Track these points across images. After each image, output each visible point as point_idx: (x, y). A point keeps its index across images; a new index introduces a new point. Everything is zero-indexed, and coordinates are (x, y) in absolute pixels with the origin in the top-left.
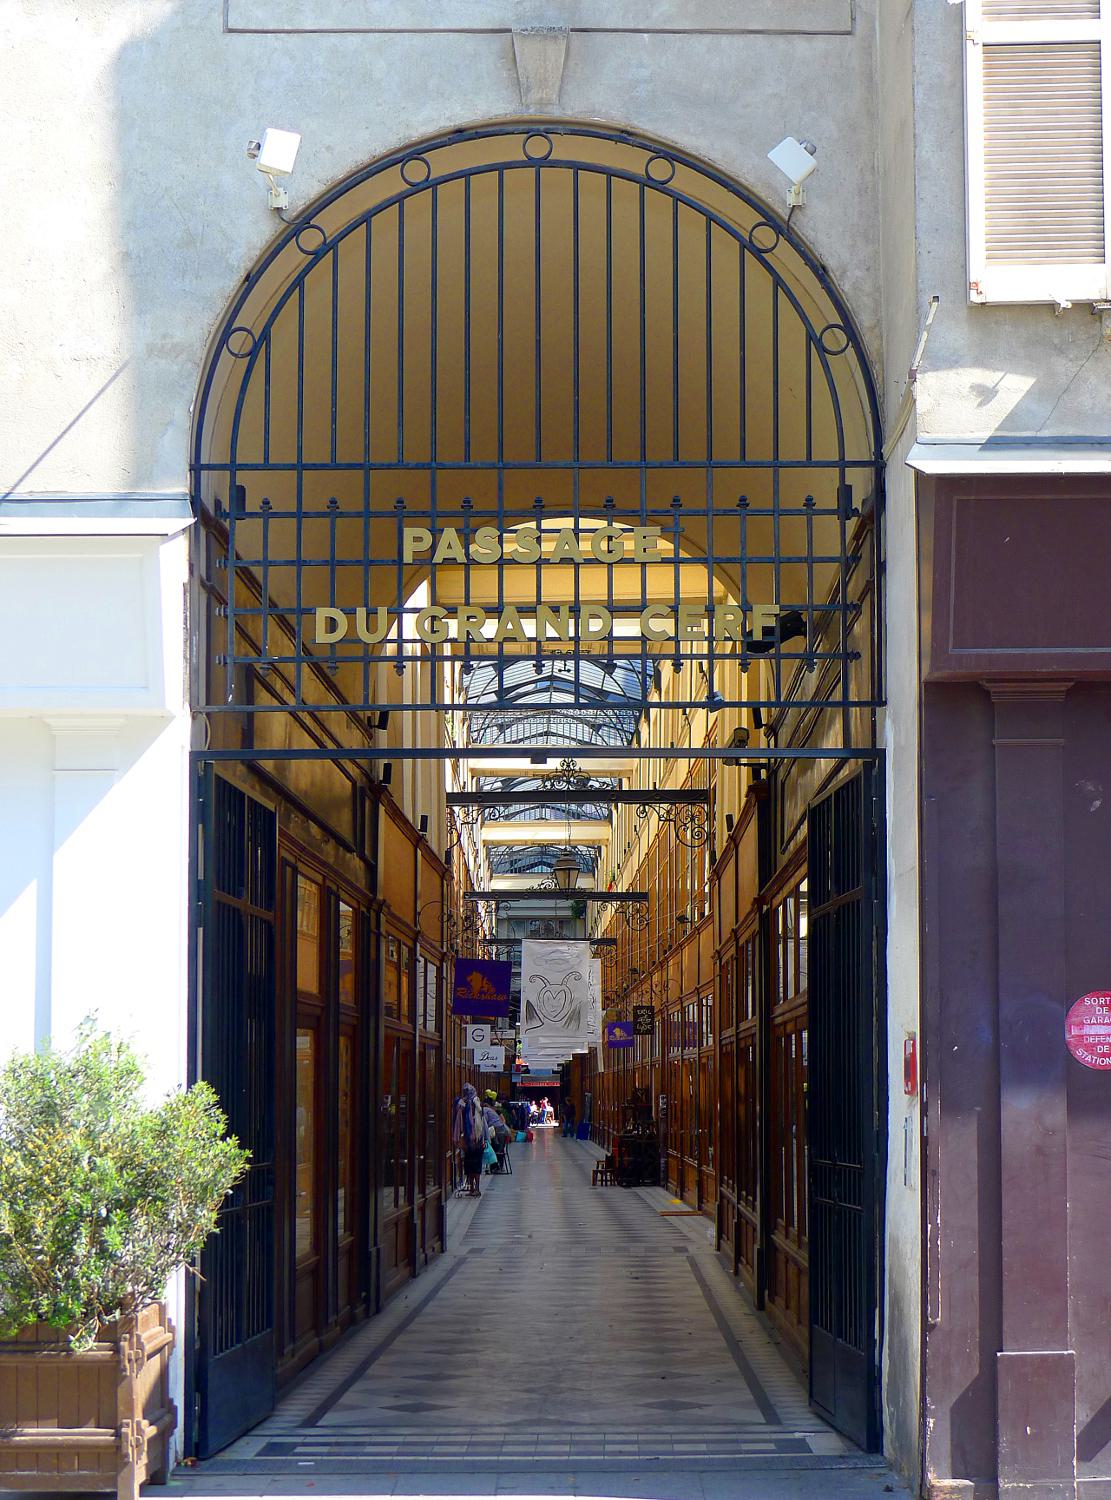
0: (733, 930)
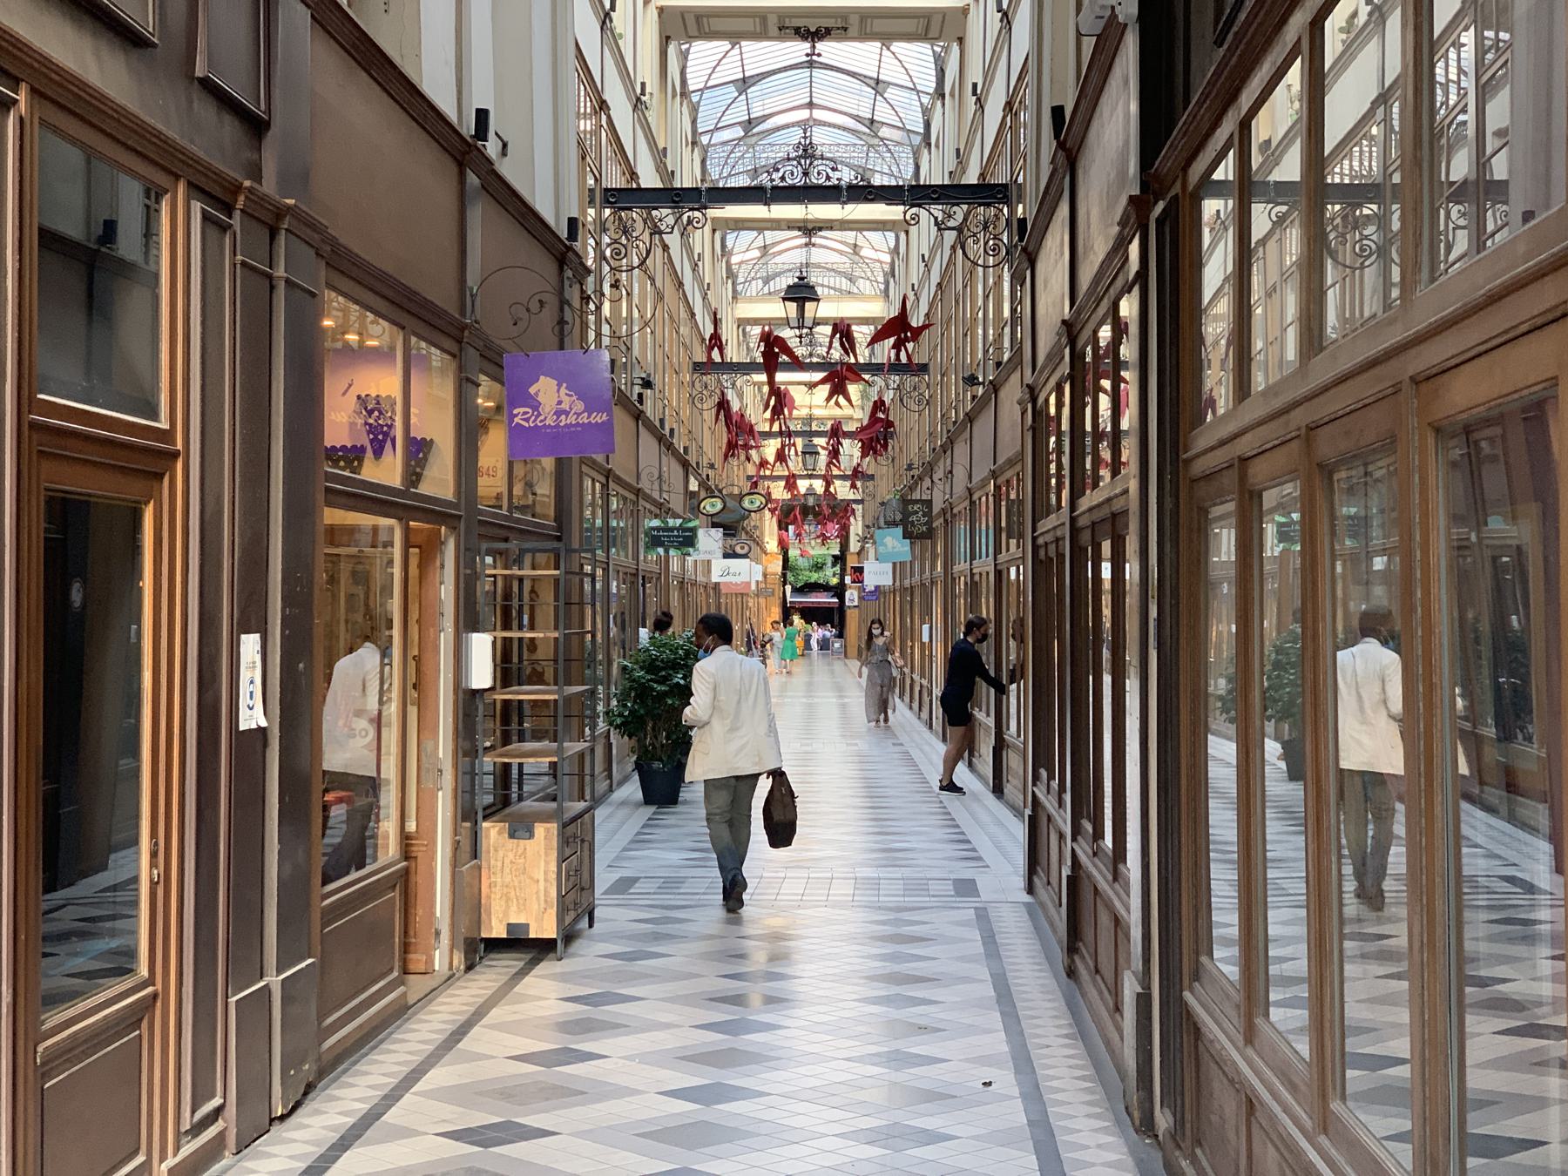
0: (1064, 322)
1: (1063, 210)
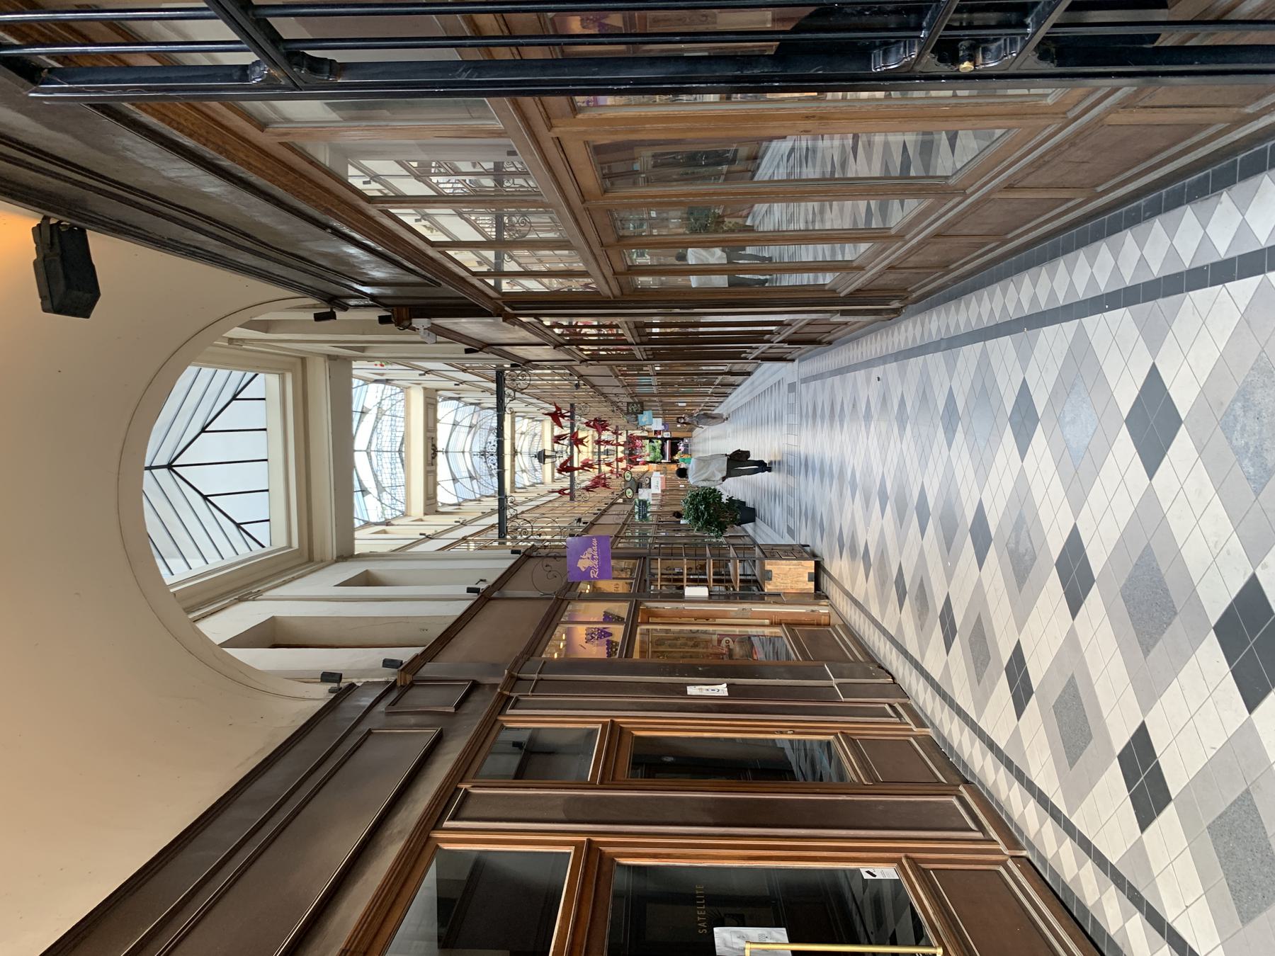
1: (506, 348)
